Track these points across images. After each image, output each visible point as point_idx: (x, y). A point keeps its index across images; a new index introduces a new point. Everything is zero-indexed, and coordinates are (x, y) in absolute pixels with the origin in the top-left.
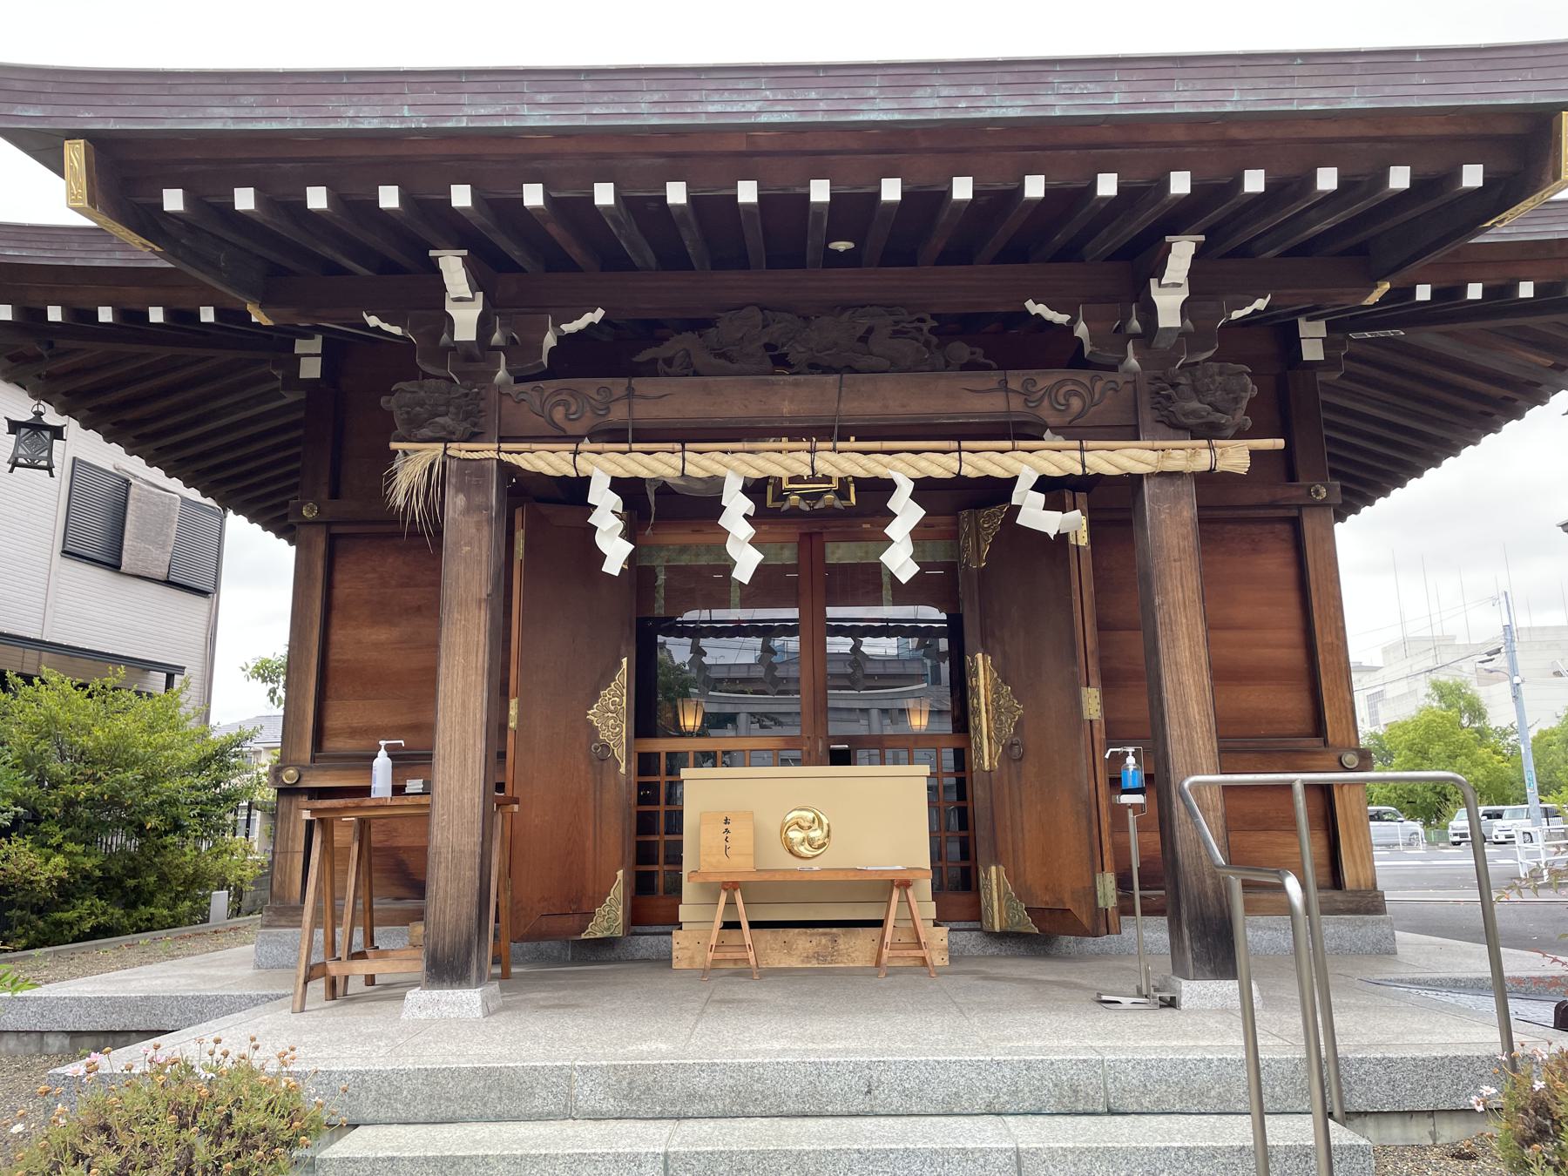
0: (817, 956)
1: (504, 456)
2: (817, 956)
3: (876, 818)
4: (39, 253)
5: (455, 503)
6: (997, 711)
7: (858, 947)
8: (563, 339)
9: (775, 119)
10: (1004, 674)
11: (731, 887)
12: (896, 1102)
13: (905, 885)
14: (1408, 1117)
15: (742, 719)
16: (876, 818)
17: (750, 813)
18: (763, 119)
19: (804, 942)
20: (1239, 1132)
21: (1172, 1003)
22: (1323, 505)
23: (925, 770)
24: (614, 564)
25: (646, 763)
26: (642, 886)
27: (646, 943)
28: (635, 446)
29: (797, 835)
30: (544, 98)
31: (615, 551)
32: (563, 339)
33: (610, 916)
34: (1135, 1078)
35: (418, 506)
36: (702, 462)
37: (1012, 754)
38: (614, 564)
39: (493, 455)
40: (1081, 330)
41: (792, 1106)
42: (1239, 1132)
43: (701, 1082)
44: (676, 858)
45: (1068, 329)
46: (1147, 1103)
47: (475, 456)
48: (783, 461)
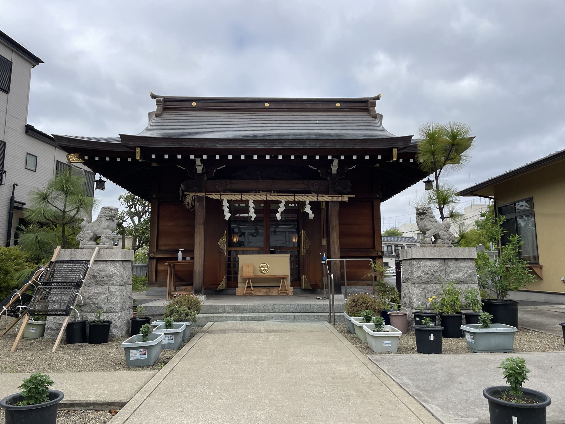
0: (266, 293)
2: (266, 293)
3: (279, 265)
5: (197, 204)
6: (306, 243)
7: (274, 292)
8: (217, 170)
10: (307, 235)
11: (249, 279)
13: (284, 279)
15: (246, 234)
16: (279, 265)
17: (252, 264)
19: (263, 290)
20: (328, 314)
22: (378, 198)
23: (289, 255)
24: (227, 218)
25: (229, 253)
26: (229, 279)
27: (230, 291)
29: (262, 269)
31: (228, 216)
32: (217, 170)
33: (223, 285)
34: (316, 307)
35: (190, 205)
36: (245, 197)
37: (308, 252)
38: (227, 218)
40: (319, 171)
41: (260, 311)
42: (328, 314)
44: (237, 273)
45: (317, 170)
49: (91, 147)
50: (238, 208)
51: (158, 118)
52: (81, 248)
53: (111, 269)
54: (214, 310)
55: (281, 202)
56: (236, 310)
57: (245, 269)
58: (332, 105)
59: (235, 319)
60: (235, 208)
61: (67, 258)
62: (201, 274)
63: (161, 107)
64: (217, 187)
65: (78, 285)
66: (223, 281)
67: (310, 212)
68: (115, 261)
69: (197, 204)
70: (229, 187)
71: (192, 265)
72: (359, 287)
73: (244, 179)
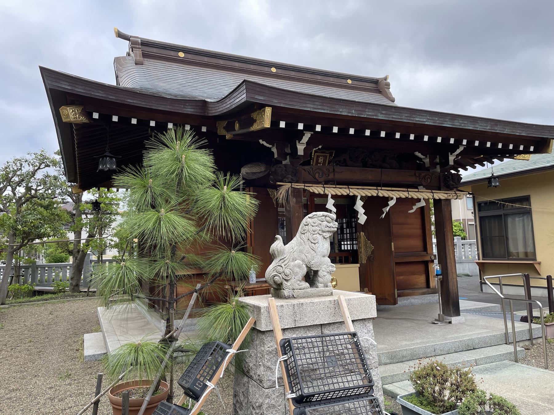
1: (306, 188)
4: (140, 102)
9: (428, 123)
12: (440, 353)
14: (306, 329)
18: (426, 123)
21: (450, 323)
23: (358, 265)
28: (337, 186)
30: (384, 112)
34: (477, 341)
39: (303, 187)
43: (405, 353)
46: (479, 347)
47: (298, 187)
48: (371, 192)
49: (112, 98)
51: (139, 66)
52: (288, 298)
55: (392, 199)
58: (344, 81)
64: (317, 176)
67: (361, 211)
68: (365, 319)
70: (331, 176)
72: (416, 297)
73: (347, 166)
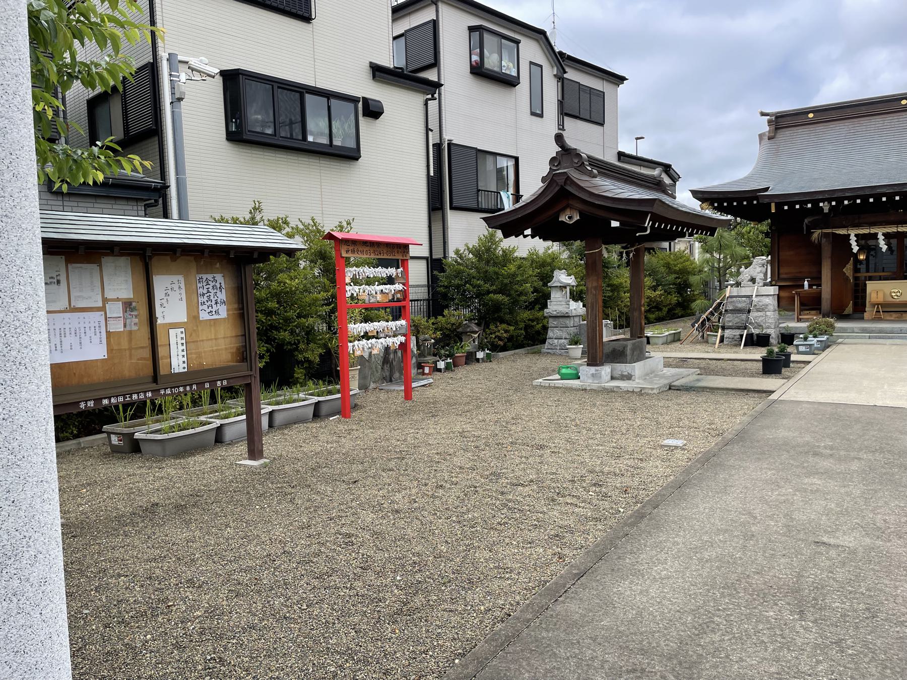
5: (824, 240)
11: (878, 304)
19: (894, 315)
25: (856, 279)
26: (855, 304)
27: (857, 315)
33: (849, 309)
44: (864, 297)
50: (866, 241)
51: (772, 141)
53: (767, 300)
54: (844, 330)
56: (864, 330)
57: (874, 296)
59: (864, 337)
60: (866, 241)
61: (735, 294)
62: (829, 302)
63: (773, 127)
65: (749, 311)
66: (851, 305)
69: (824, 240)
71: (820, 293)
